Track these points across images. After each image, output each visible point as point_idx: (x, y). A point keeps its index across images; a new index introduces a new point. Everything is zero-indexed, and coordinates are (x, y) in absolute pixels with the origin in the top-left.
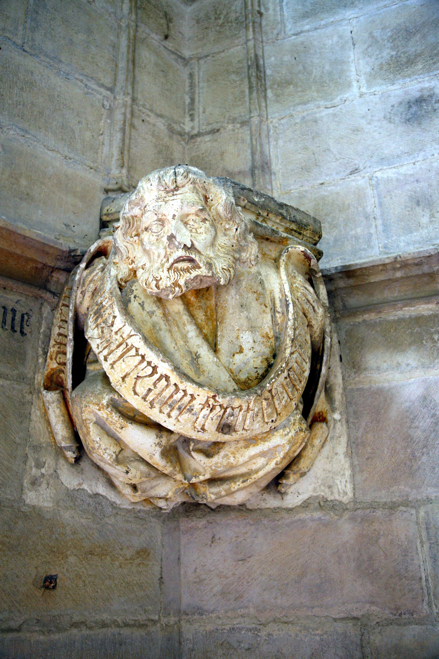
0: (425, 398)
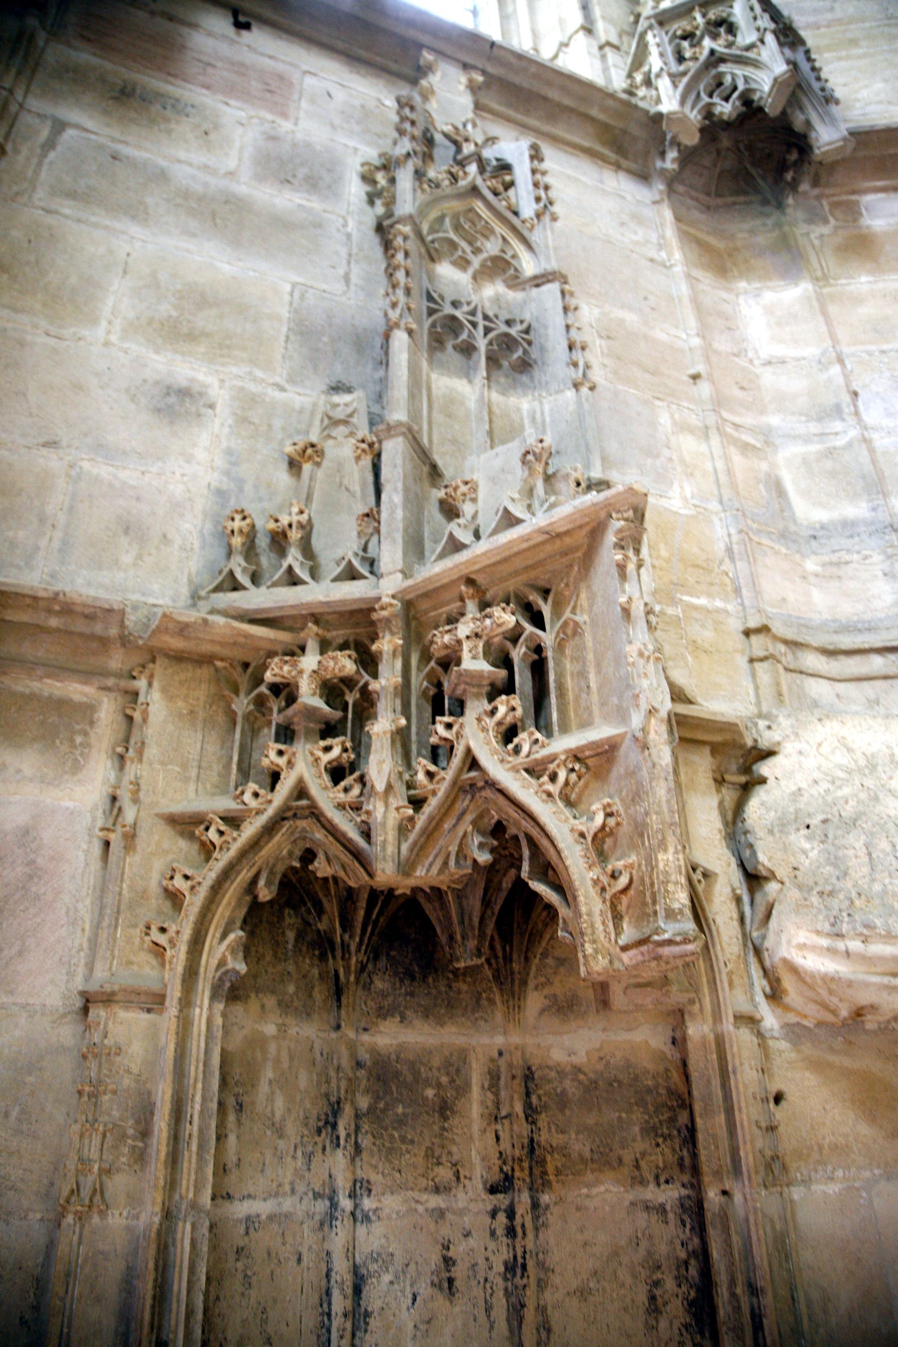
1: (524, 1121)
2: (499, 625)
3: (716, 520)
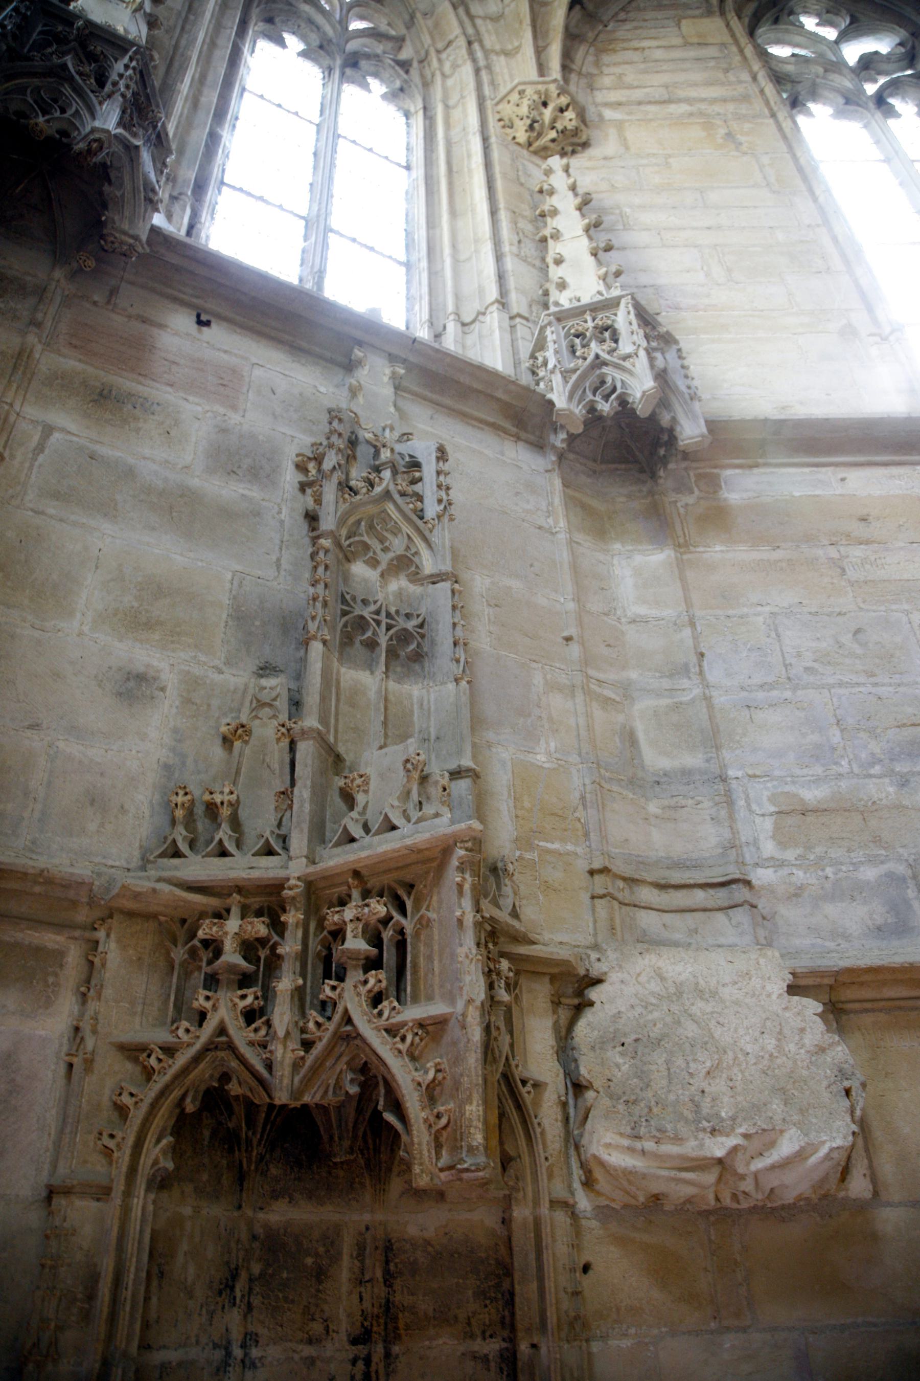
0: (9, 1056)
3: (574, 771)
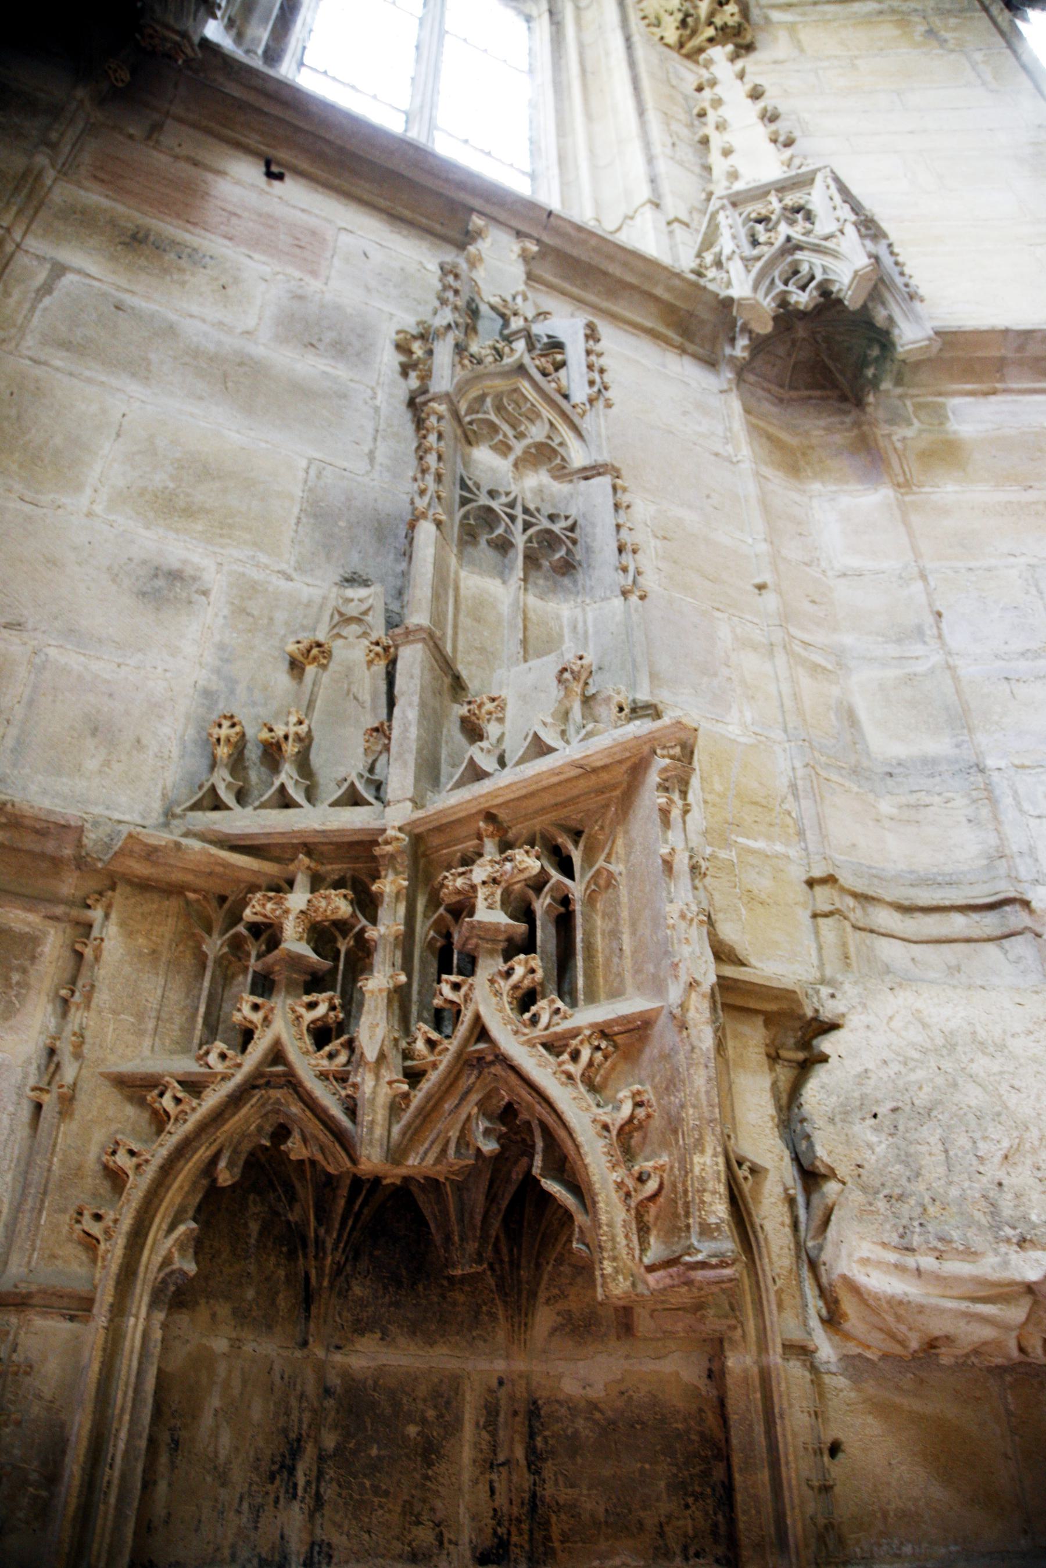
1: (525, 1470)
2: (521, 871)
